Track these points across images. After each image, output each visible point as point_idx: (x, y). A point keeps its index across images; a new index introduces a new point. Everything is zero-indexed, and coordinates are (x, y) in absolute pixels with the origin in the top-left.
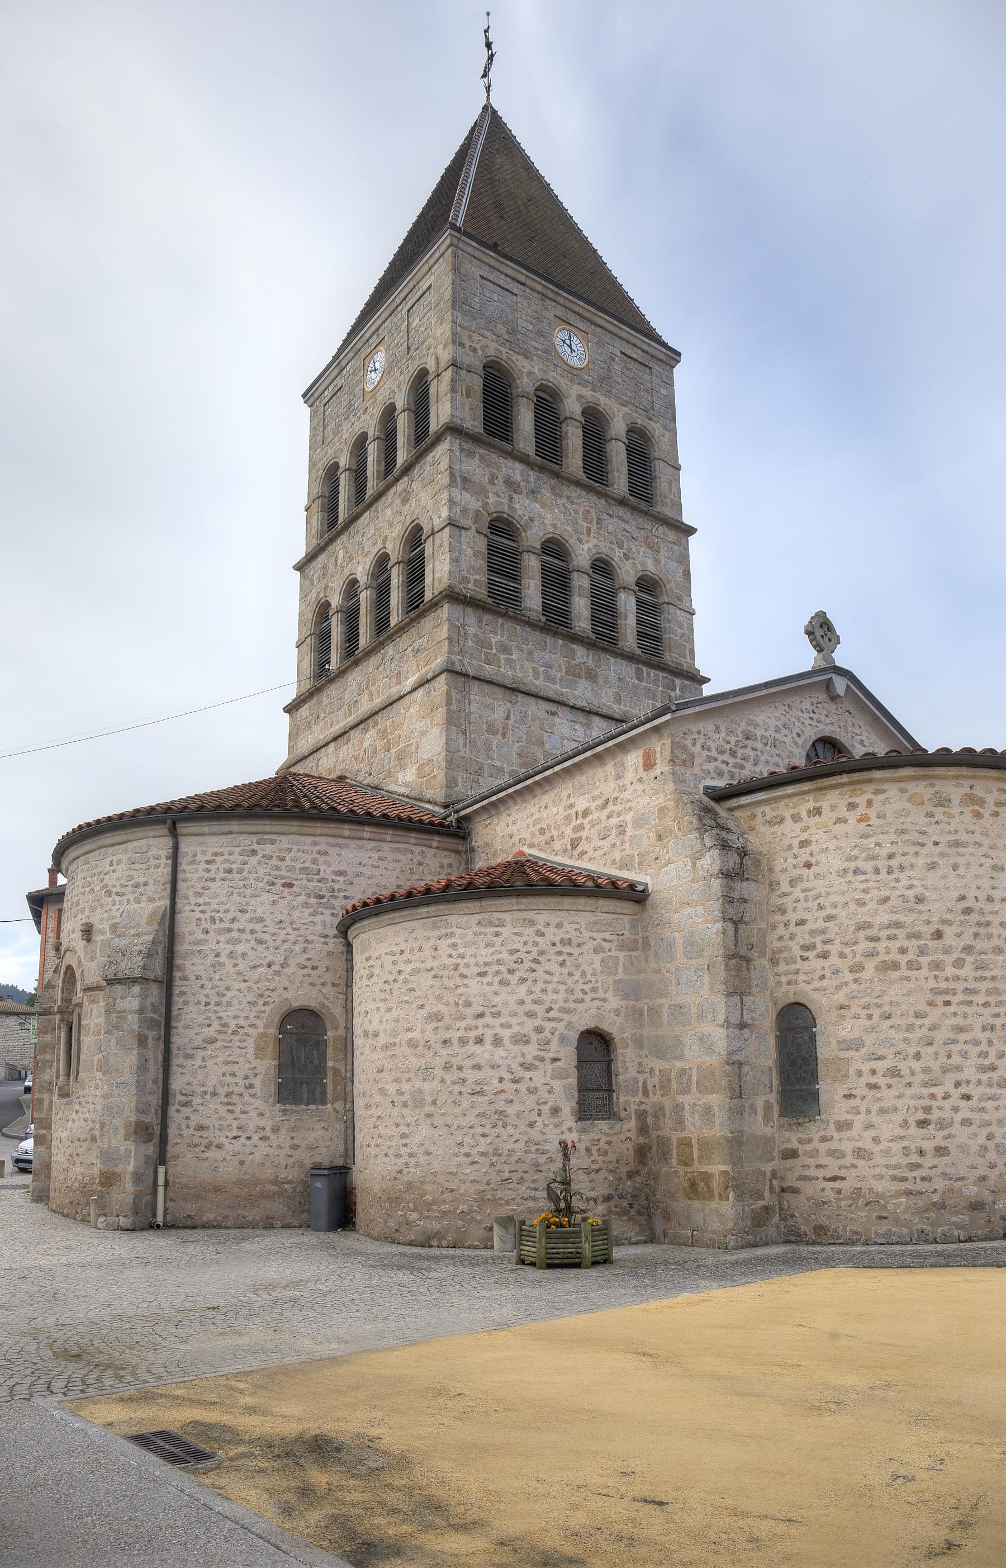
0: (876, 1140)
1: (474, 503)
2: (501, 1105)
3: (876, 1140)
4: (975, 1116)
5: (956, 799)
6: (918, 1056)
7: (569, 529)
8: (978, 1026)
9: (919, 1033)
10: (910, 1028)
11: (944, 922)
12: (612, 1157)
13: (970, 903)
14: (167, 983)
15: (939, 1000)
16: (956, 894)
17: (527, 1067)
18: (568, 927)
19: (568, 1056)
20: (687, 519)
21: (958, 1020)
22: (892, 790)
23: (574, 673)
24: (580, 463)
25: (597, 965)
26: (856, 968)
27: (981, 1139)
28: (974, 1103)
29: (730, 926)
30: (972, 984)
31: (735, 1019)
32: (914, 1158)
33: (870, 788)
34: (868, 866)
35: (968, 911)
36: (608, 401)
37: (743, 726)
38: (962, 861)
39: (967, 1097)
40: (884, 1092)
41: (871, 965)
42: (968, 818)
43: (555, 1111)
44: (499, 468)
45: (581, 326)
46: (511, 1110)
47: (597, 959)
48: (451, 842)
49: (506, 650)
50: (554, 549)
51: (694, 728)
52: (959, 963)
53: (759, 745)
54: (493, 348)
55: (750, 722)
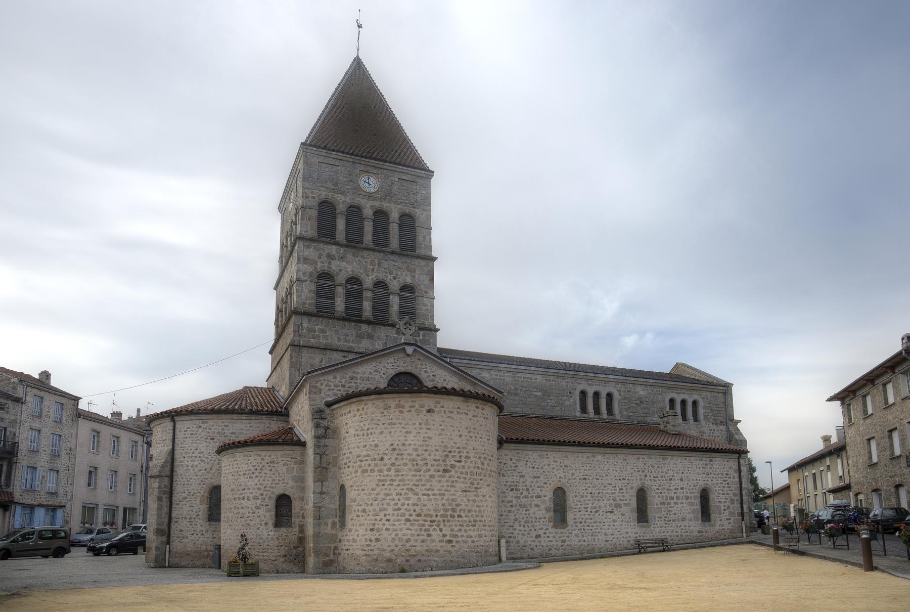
0: (358, 536)
1: (309, 268)
2: (249, 522)
3: (358, 536)
4: (391, 527)
5: (393, 406)
6: (372, 505)
7: (362, 271)
8: (394, 494)
9: (373, 496)
10: (370, 494)
11: (384, 454)
12: (287, 541)
13: (395, 446)
14: (171, 477)
15: (381, 484)
16: (389, 443)
17: (257, 508)
18: (273, 456)
19: (272, 504)
20: (434, 254)
21: (387, 491)
22: (370, 404)
23: (360, 337)
24: (371, 238)
25: (285, 470)
26: (356, 472)
27: (393, 536)
28: (391, 522)
29: (318, 457)
30: (393, 478)
31: (318, 490)
32: (369, 543)
33: (363, 403)
34: (361, 433)
35: (394, 450)
36: (389, 205)
37: (350, 374)
38: (393, 430)
39: (388, 520)
40: (361, 518)
41: (360, 470)
42: (397, 413)
43: (266, 524)
44: (324, 250)
45: (375, 171)
46: (252, 523)
47: (285, 468)
48: (282, 418)
49: (323, 331)
50: (354, 280)
51: (322, 379)
52: (389, 470)
53: (359, 381)
54: (324, 194)
55: (354, 372)
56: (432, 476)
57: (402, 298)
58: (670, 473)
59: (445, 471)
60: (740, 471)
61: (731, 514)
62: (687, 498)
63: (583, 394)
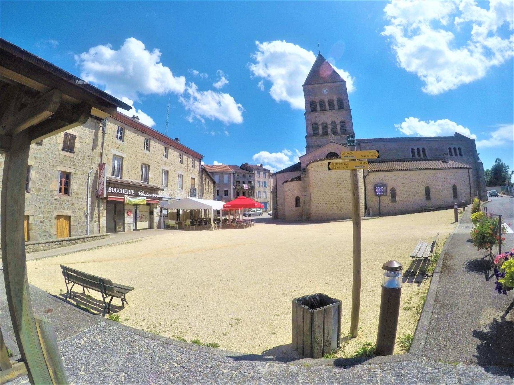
56: (333, 188)
57: (341, 125)
58: (439, 179)
59: (338, 186)
60: (469, 176)
61: (466, 194)
62: (447, 189)
63: (413, 150)
